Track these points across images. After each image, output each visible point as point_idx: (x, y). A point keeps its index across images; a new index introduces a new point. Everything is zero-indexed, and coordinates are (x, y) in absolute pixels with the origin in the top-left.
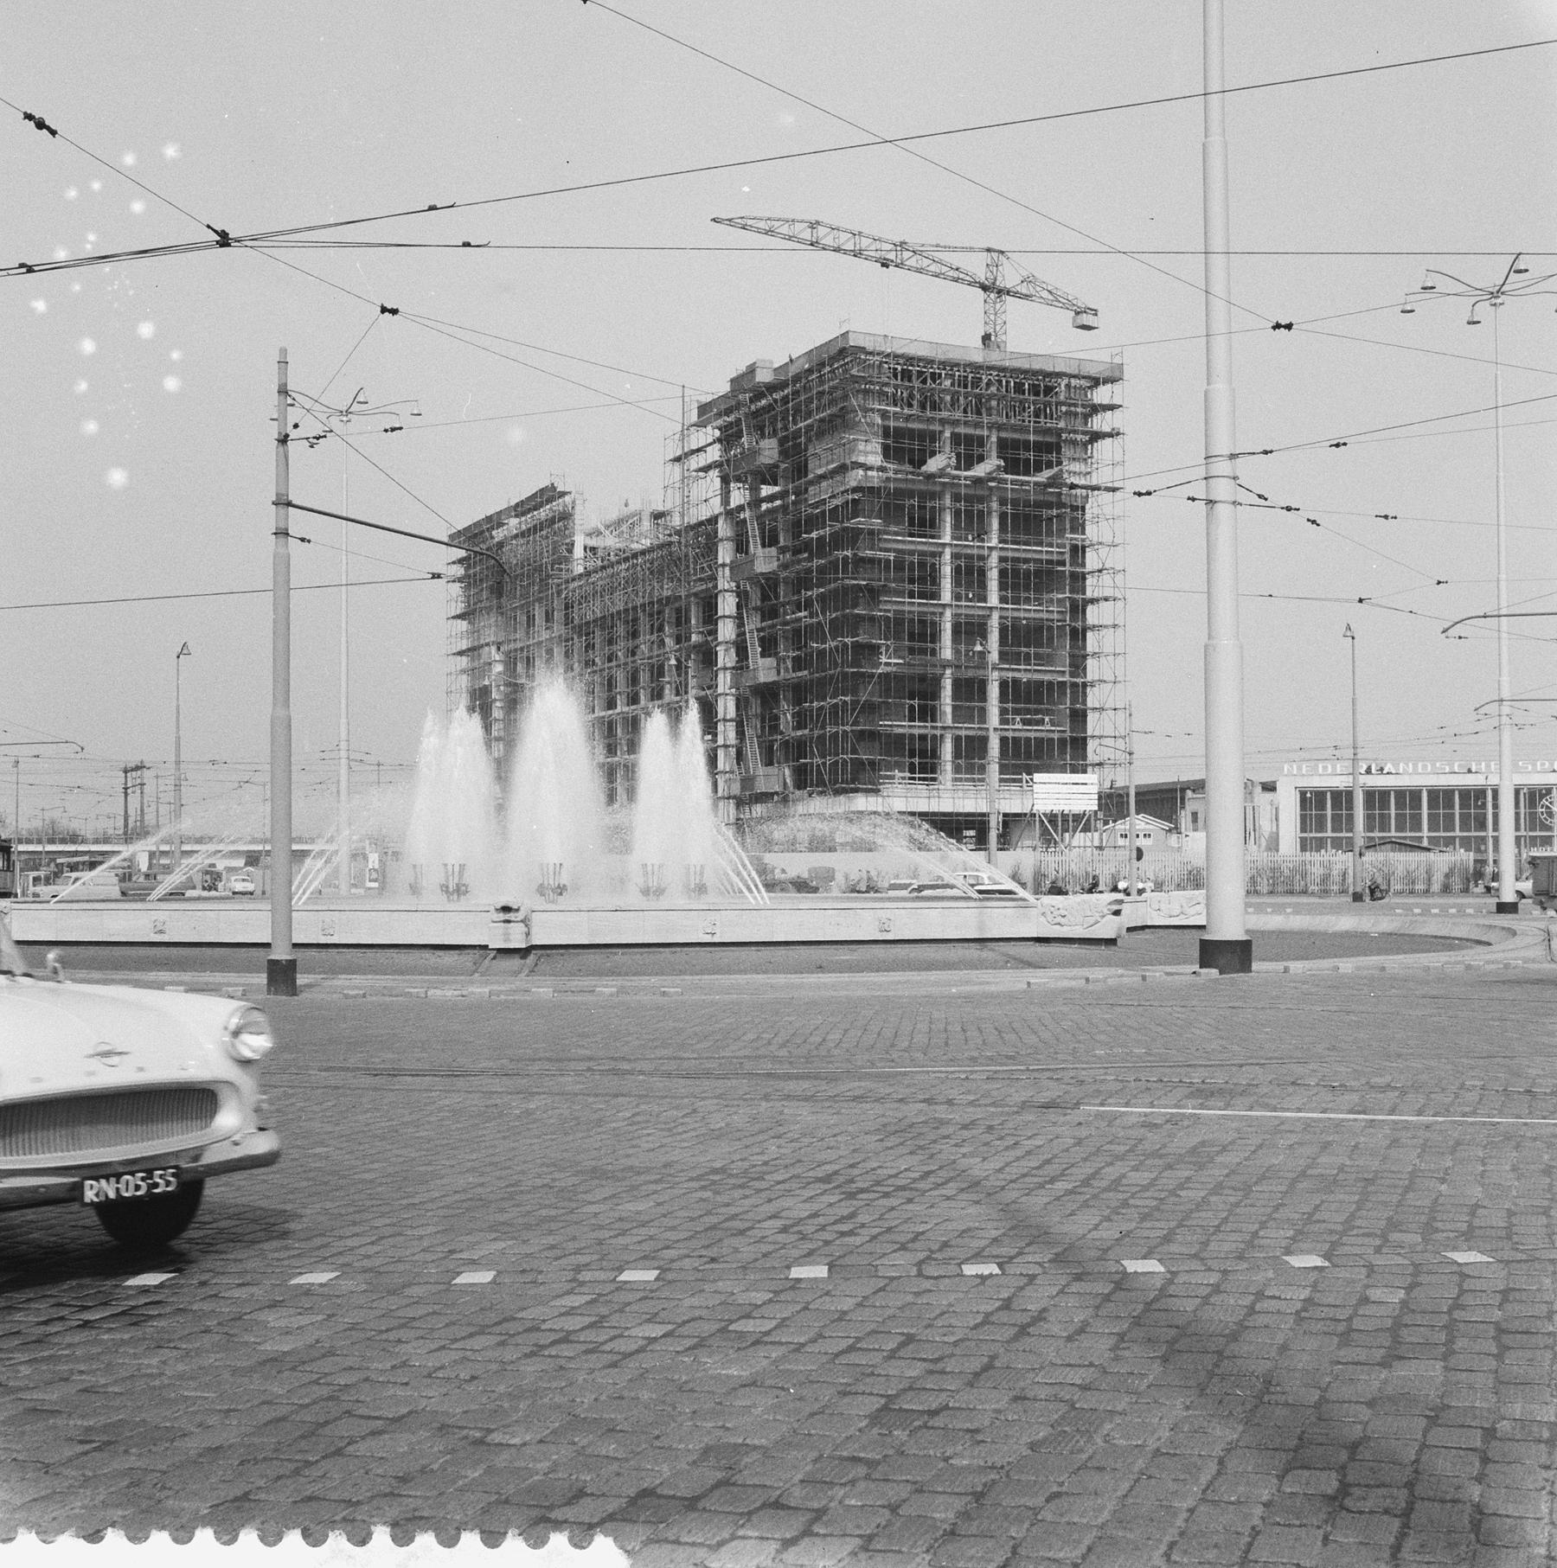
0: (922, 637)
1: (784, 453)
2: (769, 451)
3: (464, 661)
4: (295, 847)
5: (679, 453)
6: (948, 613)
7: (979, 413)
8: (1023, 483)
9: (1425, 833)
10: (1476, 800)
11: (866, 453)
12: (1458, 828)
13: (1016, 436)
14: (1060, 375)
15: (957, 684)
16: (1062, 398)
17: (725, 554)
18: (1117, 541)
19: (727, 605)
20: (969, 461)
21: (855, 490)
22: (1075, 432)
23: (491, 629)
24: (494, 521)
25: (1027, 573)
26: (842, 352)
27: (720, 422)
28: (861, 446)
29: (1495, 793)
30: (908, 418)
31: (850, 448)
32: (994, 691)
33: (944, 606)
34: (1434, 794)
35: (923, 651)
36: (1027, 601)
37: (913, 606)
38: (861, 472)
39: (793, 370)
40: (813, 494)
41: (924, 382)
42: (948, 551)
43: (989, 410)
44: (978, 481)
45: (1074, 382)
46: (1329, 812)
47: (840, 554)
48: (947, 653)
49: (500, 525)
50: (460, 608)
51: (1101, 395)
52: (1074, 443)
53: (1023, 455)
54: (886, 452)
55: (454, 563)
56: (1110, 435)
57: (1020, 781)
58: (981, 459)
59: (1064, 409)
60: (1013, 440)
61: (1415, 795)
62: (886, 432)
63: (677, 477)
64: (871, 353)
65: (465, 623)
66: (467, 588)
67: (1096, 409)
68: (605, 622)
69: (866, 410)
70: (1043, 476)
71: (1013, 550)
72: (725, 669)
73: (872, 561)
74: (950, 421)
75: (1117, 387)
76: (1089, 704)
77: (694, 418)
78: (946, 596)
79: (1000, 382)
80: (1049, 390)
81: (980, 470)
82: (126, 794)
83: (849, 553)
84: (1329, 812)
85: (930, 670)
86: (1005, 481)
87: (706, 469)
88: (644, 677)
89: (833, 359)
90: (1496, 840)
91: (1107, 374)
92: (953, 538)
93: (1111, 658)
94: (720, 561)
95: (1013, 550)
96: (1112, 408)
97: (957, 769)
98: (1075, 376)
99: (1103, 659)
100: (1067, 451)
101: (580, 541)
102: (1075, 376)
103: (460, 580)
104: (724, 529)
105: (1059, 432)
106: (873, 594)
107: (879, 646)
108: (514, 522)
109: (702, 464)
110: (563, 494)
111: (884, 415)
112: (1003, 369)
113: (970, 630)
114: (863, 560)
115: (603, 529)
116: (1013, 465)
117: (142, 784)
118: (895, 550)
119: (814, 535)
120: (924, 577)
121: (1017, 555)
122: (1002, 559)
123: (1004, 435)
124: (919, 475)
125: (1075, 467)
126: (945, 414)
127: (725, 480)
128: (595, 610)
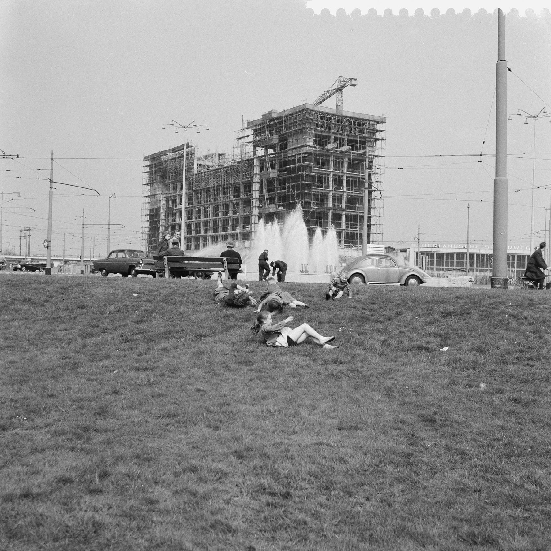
0: (321, 200)
1: (280, 140)
2: (275, 139)
3: (148, 200)
4: (52, 258)
5: (240, 137)
6: (331, 193)
7: (326, 128)
8: (355, 153)
9: (435, 266)
10: (482, 257)
11: (309, 142)
12: (485, 266)
13: (354, 139)
14: (367, 120)
15: (333, 215)
16: (367, 127)
17: (256, 170)
18: (382, 173)
19: (256, 187)
20: (341, 145)
21: (306, 153)
22: (371, 138)
23: (159, 189)
24: (164, 153)
25: (356, 181)
26: (304, 110)
27: (254, 128)
28: (308, 140)
29: (466, 254)
30: (322, 131)
31: (304, 140)
32: (344, 218)
33: (330, 191)
34: (519, 256)
35: (321, 204)
36: (355, 190)
37: (321, 190)
38: (307, 148)
39: (285, 114)
40: (289, 154)
41: (327, 120)
42: (332, 174)
43: (346, 129)
44: (342, 152)
45: (371, 123)
46: (445, 260)
47: (301, 173)
48: (330, 205)
49: (165, 154)
50: (147, 181)
51: (379, 127)
52: (371, 142)
53: (355, 145)
54: (315, 141)
55: (146, 166)
56: (381, 140)
57: (350, 246)
58: (343, 145)
59: (367, 131)
60: (353, 140)
61: (452, 255)
62: (316, 136)
63: (240, 144)
64: (313, 111)
65: (149, 186)
66: (149, 175)
67: (377, 131)
68: (207, 191)
69: (310, 128)
70: (361, 152)
71: (352, 174)
72: (255, 207)
73: (310, 176)
74: (333, 133)
75: (384, 124)
76: (372, 223)
77: (246, 126)
78: (331, 188)
79: (349, 121)
80: (363, 124)
81: (343, 149)
82: (21, 239)
83: (304, 173)
84: (445, 260)
85: (326, 211)
86: (350, 153)
87: (249, 143)
88: (221, 208)
89: (300, 111)
90: (443, 269)
91: (381, 120)
92: (333, 170)
93: (378, 209)
94: (255, 173)
95: (352, 174)
96: (382, 131)
97: (346, 242)
98: (371, 121)
99: (375, 209)
100: (368, 144)
101: (196, 162)
102: (371, 121)
103: (148, 172)
104: (256, 162)
105: (365, 138)
106: (309, 186)
107: (310, 203)
108: (171, 154)
109: (248, 141)
110: (192, 146)
111: (315, 130)
112: (350, 118)
113: (337, 199)
114: (307, 175)
115: (203, 158)
116: (354, 148)
117: (29, 236)
118: (318, 173)
119: (291, 166)
120: (322, 181)
121: (353, 176)
122: (348, 177)
123: (350, 138)
124: (324, 149)
125: (371, 149)
126: (332, 131)
127: (255, 147)
128: (203, 185)
